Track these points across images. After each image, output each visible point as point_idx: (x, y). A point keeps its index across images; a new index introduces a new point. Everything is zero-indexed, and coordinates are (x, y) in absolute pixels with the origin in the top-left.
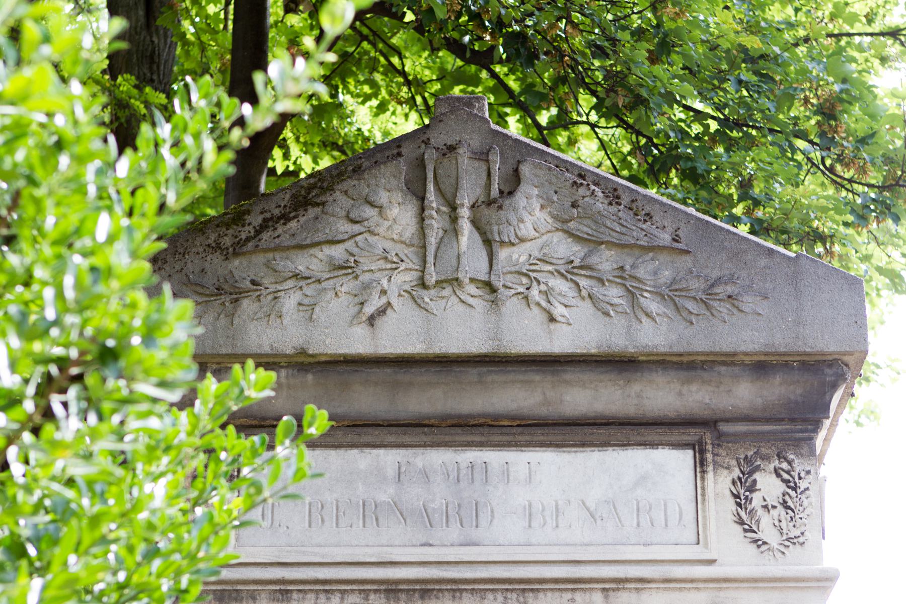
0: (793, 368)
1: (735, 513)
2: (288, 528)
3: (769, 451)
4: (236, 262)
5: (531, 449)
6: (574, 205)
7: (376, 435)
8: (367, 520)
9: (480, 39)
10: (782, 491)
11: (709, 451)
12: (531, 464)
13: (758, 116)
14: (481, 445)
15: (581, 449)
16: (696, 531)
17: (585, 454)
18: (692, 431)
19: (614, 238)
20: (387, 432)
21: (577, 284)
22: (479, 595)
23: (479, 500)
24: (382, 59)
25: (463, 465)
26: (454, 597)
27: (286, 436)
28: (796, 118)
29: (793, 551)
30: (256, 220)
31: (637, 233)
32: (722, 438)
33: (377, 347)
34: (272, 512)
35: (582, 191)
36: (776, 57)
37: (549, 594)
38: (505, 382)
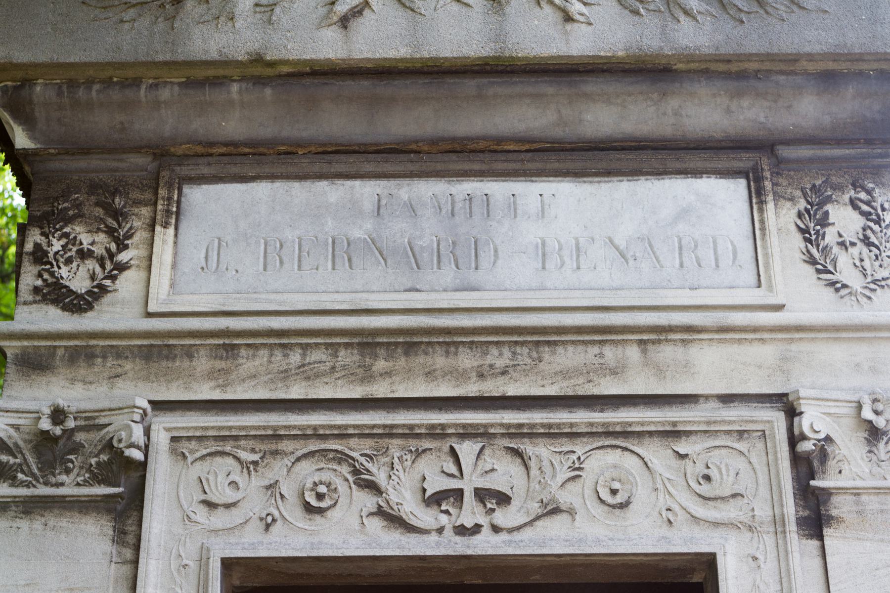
0: (869, 76)
1: (804, 250)
2: (237, 271)
3: (841, 180)
5: (544, 179)
7: (351, 163)
8: (337, 260)
10: (862, 225)
11: (767, 178)
12: (545, 196)
14: (481, 174)
15: (606, 179)
16: (755, 272)
17: (610, 184)
18: (745, 155)
20: (364, 159)
22: (479, 350)
23: (479, 236)
25: (459, 198)
26: (447, 352)
32: (782, 166)
33: (350, 51)
34: (218, 254)
37: (571, 348)
38: (511, 97)
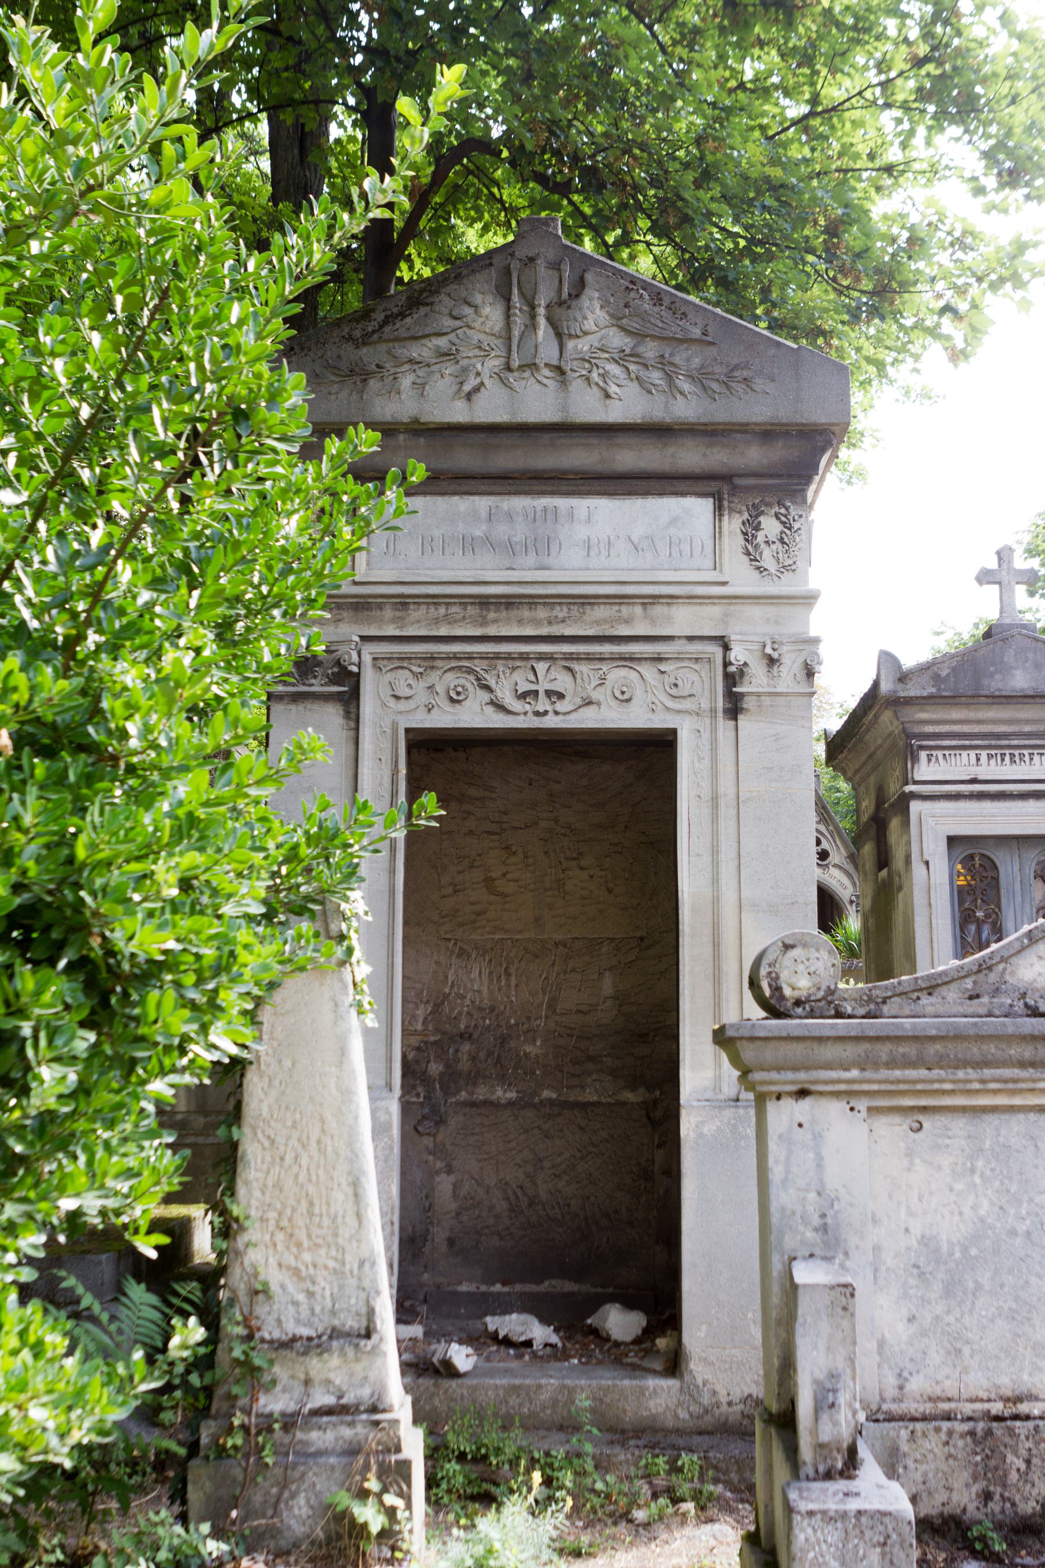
4: (365, 350)
6: (626, 306)
9: (561, 172)
13: (778, 235)
14: (553, 493)
18: (713, 483)
19: (656, 332)
21: (627, 369)
24: (485, 191)
27: (393, 483)
28: (807, 237)
29: (787, 576)
30: (379, 316)
31: (675, 329)
35: (633, 294)
36: (794, 186)
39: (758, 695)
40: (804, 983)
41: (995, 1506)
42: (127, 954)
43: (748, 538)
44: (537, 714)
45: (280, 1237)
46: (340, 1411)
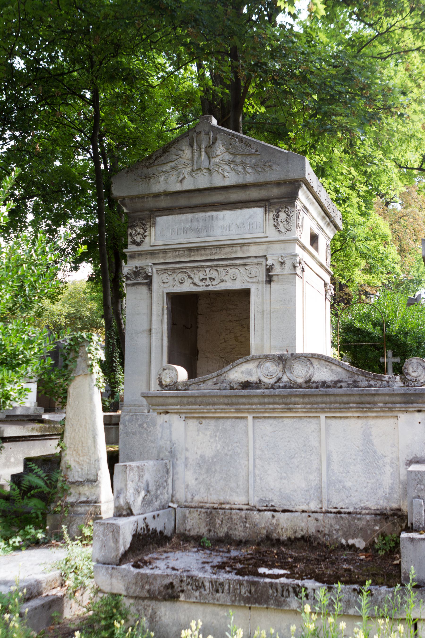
14: (211, 211)
29: (288, 233)
39: (278, 275)
40: (168, 380)
41: (212, 534)
42: (289, 356)
43: (275, 220)
44: (206, 286)
45: (74, 452)
46: (87, 502)
